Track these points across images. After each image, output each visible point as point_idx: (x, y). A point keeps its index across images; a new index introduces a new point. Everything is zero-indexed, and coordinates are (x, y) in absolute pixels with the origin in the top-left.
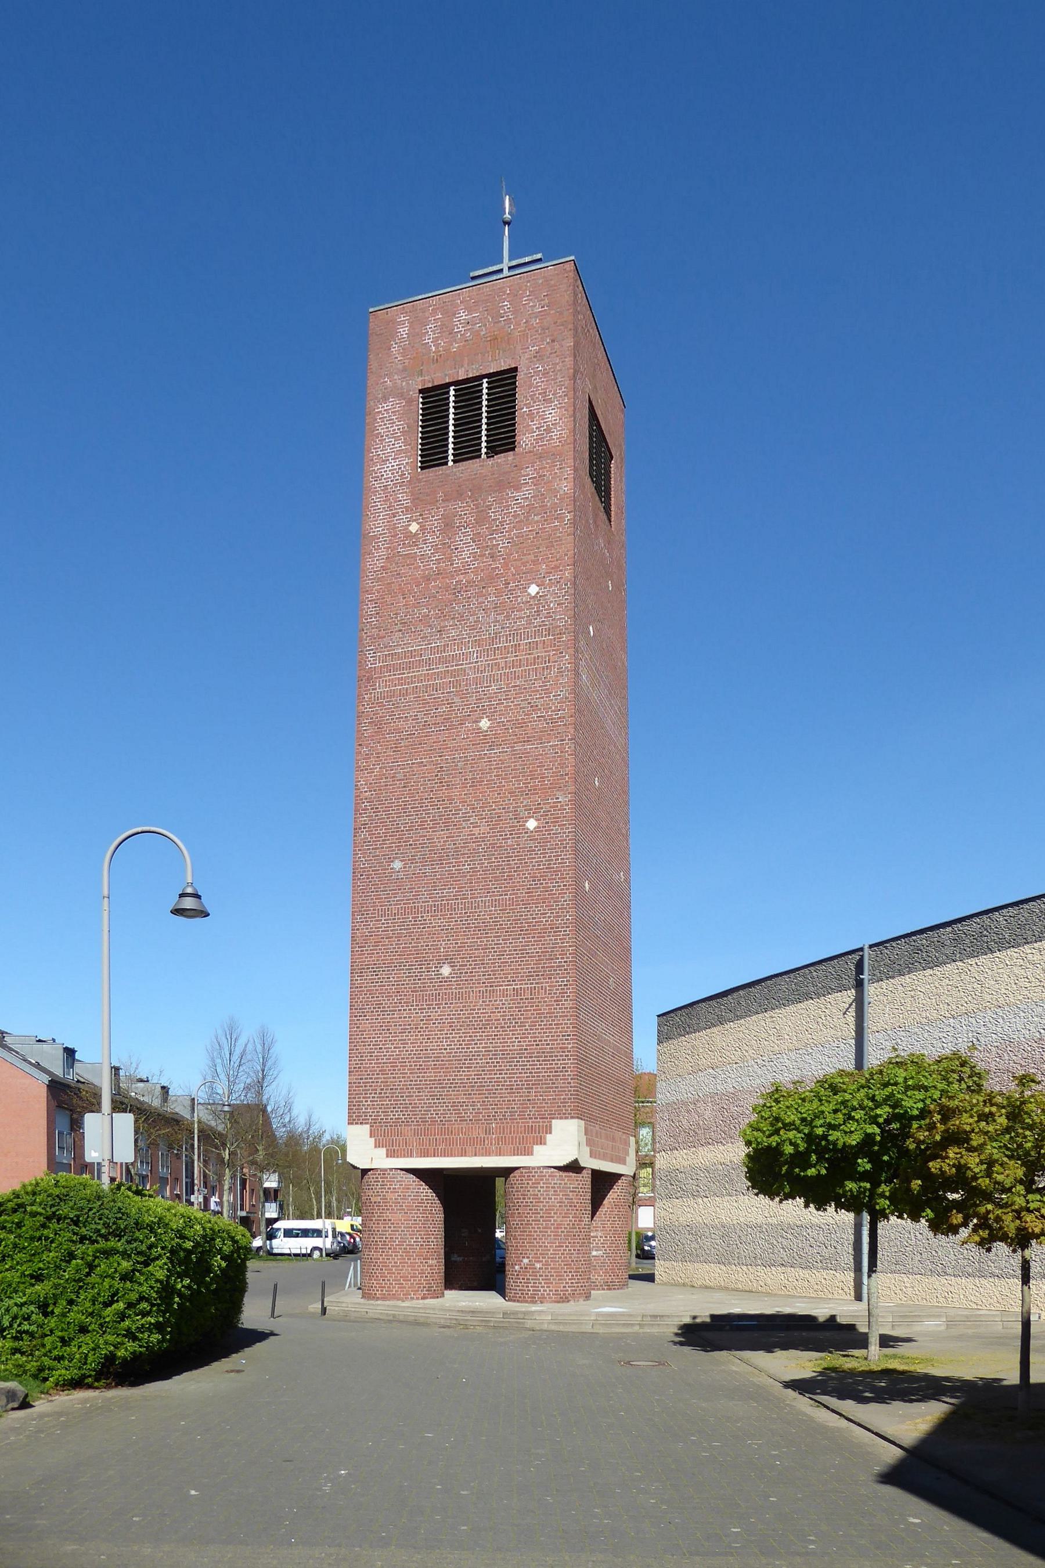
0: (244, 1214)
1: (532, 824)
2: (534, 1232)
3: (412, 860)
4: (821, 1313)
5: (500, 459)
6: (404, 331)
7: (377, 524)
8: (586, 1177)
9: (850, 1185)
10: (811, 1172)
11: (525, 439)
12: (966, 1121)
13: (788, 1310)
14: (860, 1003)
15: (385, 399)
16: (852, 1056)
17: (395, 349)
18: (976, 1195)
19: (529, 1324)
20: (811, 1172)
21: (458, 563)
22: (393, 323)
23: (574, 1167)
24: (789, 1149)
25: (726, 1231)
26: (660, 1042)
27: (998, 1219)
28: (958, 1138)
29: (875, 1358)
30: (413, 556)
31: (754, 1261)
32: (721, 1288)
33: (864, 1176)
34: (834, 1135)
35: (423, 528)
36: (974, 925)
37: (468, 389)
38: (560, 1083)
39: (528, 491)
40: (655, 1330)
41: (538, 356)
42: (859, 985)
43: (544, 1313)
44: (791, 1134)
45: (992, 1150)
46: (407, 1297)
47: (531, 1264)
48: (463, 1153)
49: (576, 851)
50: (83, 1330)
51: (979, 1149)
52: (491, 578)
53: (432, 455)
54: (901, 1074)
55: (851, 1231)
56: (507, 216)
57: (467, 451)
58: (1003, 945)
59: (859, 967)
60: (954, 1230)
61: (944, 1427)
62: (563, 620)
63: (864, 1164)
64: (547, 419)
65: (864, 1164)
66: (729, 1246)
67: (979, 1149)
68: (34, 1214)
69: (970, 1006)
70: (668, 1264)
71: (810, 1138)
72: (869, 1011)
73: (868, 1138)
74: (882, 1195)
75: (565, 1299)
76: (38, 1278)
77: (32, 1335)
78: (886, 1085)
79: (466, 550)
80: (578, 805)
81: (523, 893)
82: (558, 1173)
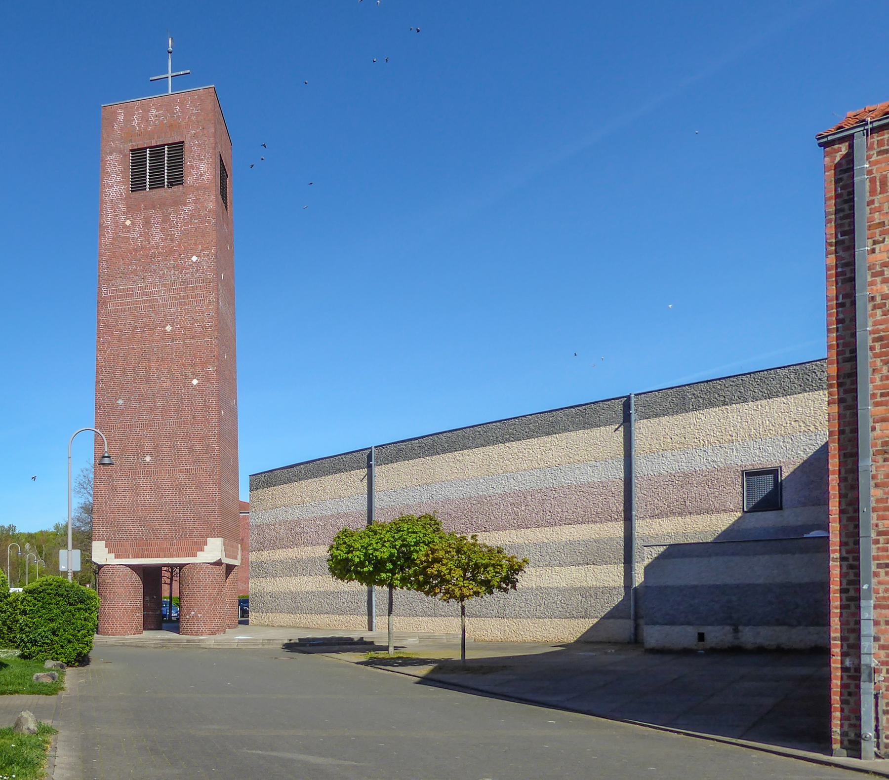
1: (195, 382)
2: (204, 606)
3: (129, 400)
6: (121, 118)
7: (108, 221)
9: (383, 575)
10: (366, 569)
11: (189, 180)
12: (441, 554)
13: (337, 636)
15: (111, 153)
16: (366, 504)
18: (444, 581)
19: (203, 645)
20: (366, 569)
21: (152, 243)
22: (115, 113)
23: (218, 563)
25: (294, 596)
26: (251, 490)
27: (453, 590)
28: (438, 560)
29: (392, 653)
30: (128, 238)
31: (310, 611)
32: (294, 627)
34: (377, 553)
35: (133, 223)
36: (429, 440)
37: (157, 152)
38: (211, 519)
39: (191, 207)
41: (195, 136)
42: (370, 467)
44: (358, 553)
46: (125, 633)
47: (196, 615)
49: (219, 396)
50: (69, 642)
51: (446, 565)
52: (171, 252)
53: (137, 185)
54: (406, 526)
55: (366, 595)
56: (170, 49)
57: (157, 183)
58: (445, 451)
59: (369, 457)
62: (210, 275)
64: (200, 169)
65: (389, 566)
66: (295, 603)
67: (446, 565)
68: (49, 594)
69: (428, 481)
70: (257, 614)
71: (365, 554)
73: (392, 555)
74: (397, 579)
75: (213, 635)
76: (52, 620)
77: (47, 643)
78: (399, 531)
79: (157, 237)
80: (219, 371)
82: (210, 566)
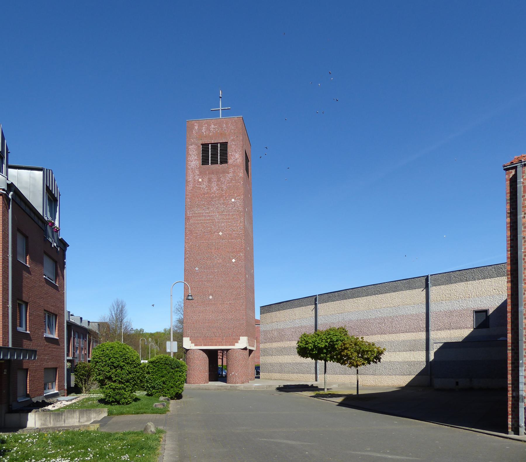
0: (70, 358)
1: (234, 260)
4: (310, 384)
5: (223, 165)
6: (196, 127)
8: (248, 350)
9: (322, 355)
10: (314, 352)
11: (230, 161)
12: (348, 346)
14: (316, 308)
15: (191, 145)
17: (194, 132)
18: (349, 358)
20: (314, 352)
22: (193, 125)
23: (245, 349)
24: (310, 348)
25: (281, 365)
26: (261, 314)
28: (346, 349)
29: (326, 392)
31: (289, 372)
33: (325, 353)
35: (203, 181)
36: (343, 293)
40: (270, 389)
41: (233, 140)
42: (316, 304)
43: (241, 386)
45: (352, 351)
46: (200, 383)
47: (234, 374)
48: (216, 345)
49: (245, 268)
50: (172, 387)
52: (222, 196)
53: (205, 161)
57: (215, 162)
58: (349, 298)
60: (345, 364)
61: (344, 400)
62: (241, 209)
63: (325, 351)
64: (235, 156)
65: (325, 351)
67: (350, 351)
71: (314, 345)
72: (318, 311)
73: (326, 346)
75: (241, 383)
76: (163, 377)
81: (231, 278)
